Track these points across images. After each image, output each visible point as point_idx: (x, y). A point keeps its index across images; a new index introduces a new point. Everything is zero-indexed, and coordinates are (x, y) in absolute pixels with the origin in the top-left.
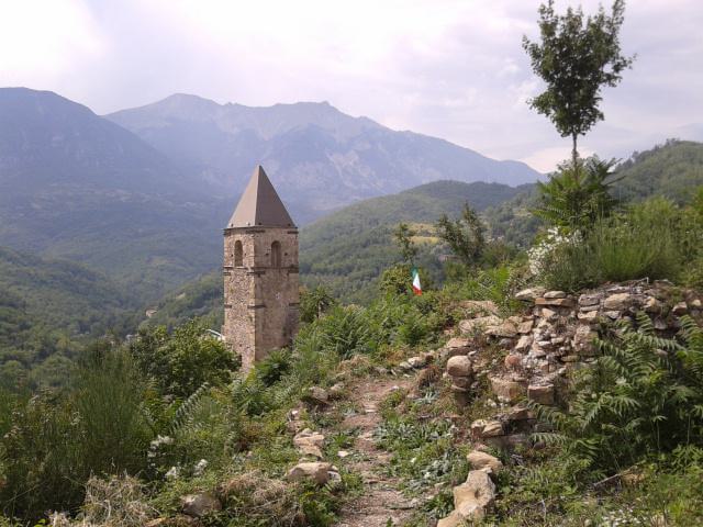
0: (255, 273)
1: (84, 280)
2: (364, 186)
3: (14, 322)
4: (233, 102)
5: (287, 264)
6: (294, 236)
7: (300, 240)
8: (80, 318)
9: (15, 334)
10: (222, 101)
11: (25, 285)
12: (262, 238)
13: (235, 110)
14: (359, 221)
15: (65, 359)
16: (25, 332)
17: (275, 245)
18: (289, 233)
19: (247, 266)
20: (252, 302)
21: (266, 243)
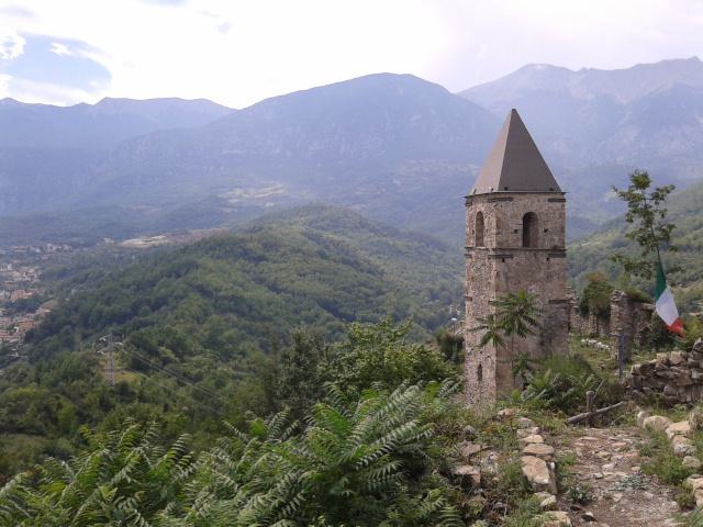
0: (497, 257)
1: (437, 251)
3: (371, 288)
4: (588, 67)
5: (548, 245)
6: (559, 205)
7: (568, 214)
8: (431, 286)
9: (371, 298)
10: (576, 67)
11: (384, 253)
13: (590, 75)
15: (414, 324)
16: (381, 297)
17: (529, 219)
18: (550, 200)
19: (489, 247)
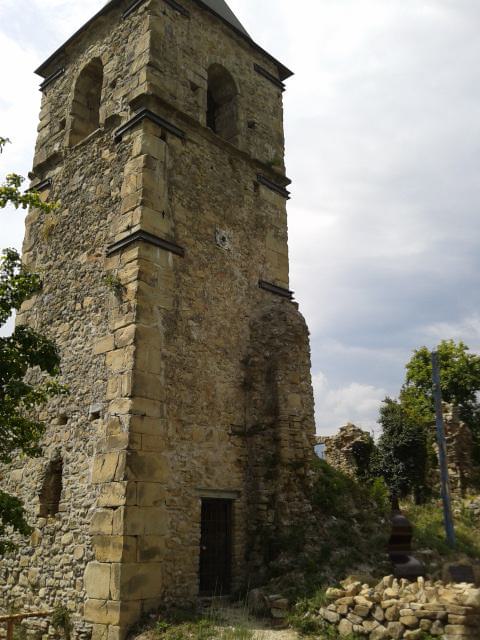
20: (128, 221)
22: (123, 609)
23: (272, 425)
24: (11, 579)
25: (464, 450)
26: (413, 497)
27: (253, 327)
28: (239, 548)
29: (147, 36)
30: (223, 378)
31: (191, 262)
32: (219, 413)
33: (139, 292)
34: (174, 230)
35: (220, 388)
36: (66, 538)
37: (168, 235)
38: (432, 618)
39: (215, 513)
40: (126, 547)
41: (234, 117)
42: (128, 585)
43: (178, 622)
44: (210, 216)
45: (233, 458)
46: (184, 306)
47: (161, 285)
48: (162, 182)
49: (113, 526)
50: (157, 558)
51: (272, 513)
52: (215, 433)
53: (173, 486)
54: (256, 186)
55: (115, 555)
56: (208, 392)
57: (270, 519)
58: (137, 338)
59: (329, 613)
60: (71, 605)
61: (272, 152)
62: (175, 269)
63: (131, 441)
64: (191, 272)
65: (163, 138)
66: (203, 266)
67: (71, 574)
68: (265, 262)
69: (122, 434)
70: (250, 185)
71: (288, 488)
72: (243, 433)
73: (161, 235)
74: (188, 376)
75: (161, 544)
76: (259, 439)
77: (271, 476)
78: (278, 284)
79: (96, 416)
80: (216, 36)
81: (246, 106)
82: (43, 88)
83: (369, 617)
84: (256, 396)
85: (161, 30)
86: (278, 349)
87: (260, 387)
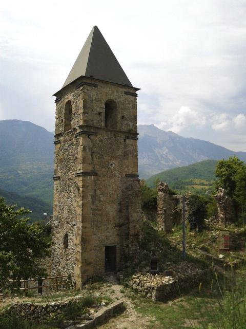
1: (39, 206)
2: (170, 163)
5: (124, 129)
12: (94, 93)
14: (168, 179)
17: (110, 106)
18: (126, 93)
20: (79, 168)
21: (98, 100)
22: (82, 278)
23: (127, 223)
24: (58, 265)
25: (227, 207)
26: (197, 229)
27: (122, 191)
28: (118, 259)
29: (82, 101)
30: (112, 210)
31: (100, 176)
32: (111, 221)
33: (83, 191)
34: (94, 168)
35: (111, 213)
36: (70, 257)
37: (92, 170)
38: (151, 288)
39: (110, 251)
40: (82, 263)
41: (116, 116)
42: (83, 272)
43: (95, 282)
44: (106, 158)
45: (116, 233)
46: (98, 192)
47: (90, 187)
48: (89, 153)
49: (79, 257)
50: (92, 264)
51: (127, 249)
52: (110, 227)
53: (96, 244)
54: (125, 140)
55: (80, 265)
56: (107, 216)
57: (127, 250)
58: (83, 205)
59: (131, 282)
60: (72, 275)
61: (131, 124)
62: (95, 181)
63: (82, 235)
64: (100, 179)
65: (89, 137)
66: (104, 176)
67: (71, 267)
68: (128, 167)
69: (80, 233)
70: (122, 141)
71: (132, 242)
72: (119, 226)
73: (90, 171)
74: (100, 213)
75: (92, 261)
76: (124, 228)
77: (127, 239)
78: (133, 173)
79: (75, 225)
80: (108, 89)
81: (121, 111)
82: (57, 101)
83: (138, 285)
84: (123, 215)
85: (87, 97)
86: (130, 199)
87: (124, 211)
